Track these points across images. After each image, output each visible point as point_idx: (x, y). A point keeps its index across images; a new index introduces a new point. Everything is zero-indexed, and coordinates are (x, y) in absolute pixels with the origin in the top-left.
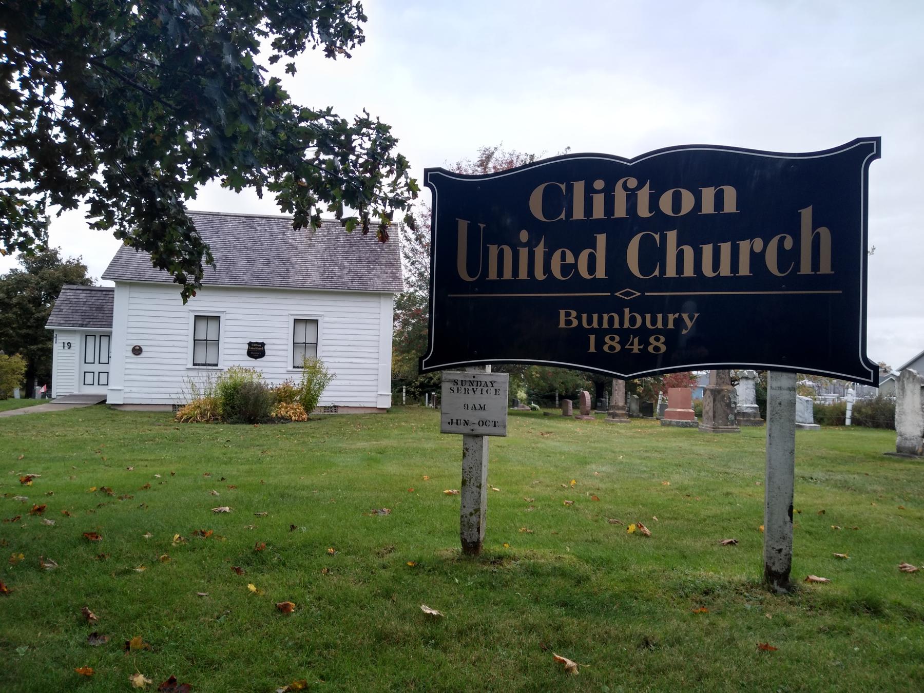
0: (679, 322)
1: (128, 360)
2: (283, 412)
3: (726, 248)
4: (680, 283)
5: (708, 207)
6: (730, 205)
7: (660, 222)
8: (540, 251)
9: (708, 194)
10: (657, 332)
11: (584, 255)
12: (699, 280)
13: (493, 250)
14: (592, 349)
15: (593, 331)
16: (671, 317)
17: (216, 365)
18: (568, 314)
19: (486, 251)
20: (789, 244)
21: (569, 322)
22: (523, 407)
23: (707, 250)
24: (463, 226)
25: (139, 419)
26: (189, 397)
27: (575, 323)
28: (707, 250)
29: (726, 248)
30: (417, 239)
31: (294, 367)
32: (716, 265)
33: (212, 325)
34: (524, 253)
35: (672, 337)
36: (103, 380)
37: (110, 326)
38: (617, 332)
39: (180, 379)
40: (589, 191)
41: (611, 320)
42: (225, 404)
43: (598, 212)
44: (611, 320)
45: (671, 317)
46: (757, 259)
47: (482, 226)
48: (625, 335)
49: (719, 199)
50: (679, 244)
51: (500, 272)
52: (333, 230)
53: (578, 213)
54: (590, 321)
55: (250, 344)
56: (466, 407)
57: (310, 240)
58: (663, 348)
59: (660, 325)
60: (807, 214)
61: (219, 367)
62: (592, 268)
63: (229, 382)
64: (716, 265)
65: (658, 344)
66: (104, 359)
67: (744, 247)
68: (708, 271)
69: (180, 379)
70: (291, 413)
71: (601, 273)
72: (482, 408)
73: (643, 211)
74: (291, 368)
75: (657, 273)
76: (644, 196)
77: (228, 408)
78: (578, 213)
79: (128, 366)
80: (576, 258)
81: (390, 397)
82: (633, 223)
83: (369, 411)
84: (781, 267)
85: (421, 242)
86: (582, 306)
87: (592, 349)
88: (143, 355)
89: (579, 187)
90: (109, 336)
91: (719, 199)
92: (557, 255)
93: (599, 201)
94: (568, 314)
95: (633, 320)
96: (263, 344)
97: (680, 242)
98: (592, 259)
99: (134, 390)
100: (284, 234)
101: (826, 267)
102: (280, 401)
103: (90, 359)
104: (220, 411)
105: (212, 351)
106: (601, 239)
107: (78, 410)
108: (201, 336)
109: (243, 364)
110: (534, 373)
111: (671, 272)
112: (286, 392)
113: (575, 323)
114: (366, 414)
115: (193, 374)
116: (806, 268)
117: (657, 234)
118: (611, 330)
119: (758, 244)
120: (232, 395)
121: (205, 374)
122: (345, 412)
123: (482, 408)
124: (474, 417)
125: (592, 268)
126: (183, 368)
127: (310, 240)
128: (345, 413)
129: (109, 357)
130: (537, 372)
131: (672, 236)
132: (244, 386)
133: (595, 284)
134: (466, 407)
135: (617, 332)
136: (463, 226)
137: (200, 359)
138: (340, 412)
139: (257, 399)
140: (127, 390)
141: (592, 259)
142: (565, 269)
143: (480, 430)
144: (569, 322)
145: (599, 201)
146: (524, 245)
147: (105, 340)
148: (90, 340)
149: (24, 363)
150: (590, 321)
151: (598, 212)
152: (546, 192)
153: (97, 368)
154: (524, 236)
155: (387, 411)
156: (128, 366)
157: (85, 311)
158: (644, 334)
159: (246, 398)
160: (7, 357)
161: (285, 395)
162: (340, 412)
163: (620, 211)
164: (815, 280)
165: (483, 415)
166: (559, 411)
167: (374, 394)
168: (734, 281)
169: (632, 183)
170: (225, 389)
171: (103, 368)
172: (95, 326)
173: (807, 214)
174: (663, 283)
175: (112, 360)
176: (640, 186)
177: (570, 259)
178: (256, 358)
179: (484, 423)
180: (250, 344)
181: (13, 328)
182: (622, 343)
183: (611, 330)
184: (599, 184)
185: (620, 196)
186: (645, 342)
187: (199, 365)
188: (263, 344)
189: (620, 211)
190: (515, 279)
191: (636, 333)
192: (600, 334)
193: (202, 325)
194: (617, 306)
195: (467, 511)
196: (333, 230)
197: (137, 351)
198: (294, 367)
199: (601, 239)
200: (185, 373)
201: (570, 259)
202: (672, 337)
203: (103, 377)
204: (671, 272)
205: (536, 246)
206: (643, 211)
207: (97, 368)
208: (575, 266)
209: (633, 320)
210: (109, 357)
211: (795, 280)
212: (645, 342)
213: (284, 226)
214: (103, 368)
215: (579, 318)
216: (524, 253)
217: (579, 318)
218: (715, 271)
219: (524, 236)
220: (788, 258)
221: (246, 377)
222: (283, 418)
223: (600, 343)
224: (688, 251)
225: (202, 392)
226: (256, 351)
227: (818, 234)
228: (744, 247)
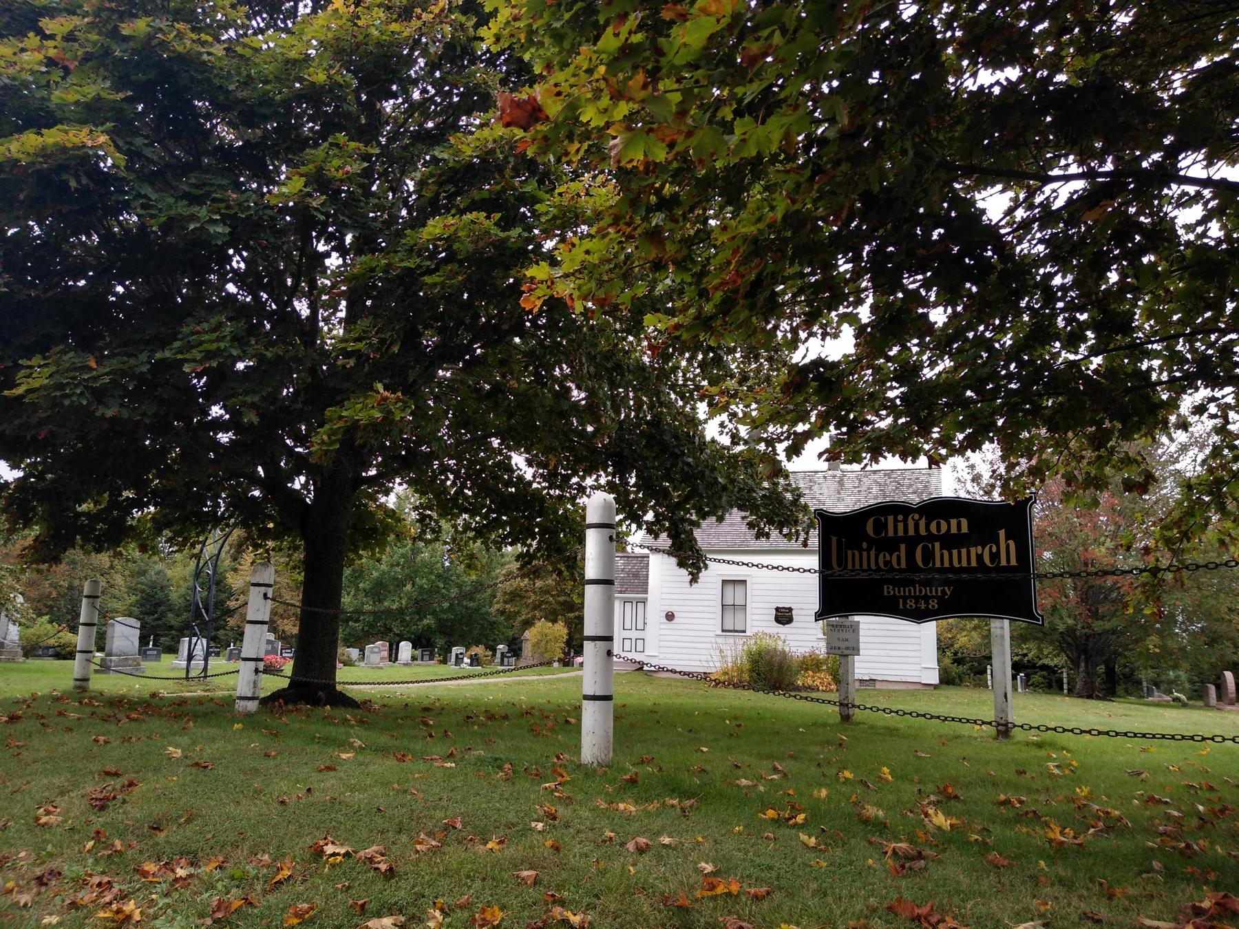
0: (944, 592)
1: (662, 626)
2: (809, 681)
3: (964, 551)
4: (942, 570)
5: (954, 530)
6: (965, 529)
7: (931, 538)
8: (873, 553)
9: (954, 522)
10: (933, 597)
11: (895, 555)
12: (952, 569)
13: (850, 553)
14: (901, 607)
15: (901, 597)
16: (939, 589)
17: (744, 632)
19: (846, 553)
20: (994, 549)
21: (889, 592)
22: (1160, 697)
23: (955, 552)
24: (834, 540)
25: (673, 683)
26: (718, 664)
27: (892, 593)
28: (955, 552)
29: (964, 551)
30: (973, 480)
31: (723, 631)
32: (960, 561)
33: (739, 589)
34: (865, 554)
35: (940, 599)
36: (640, 648)
37: (646, 592)
38: (913, 597)
39: (709, 646)
40: (896, 521)
41: (910, 590)
42: (752, 671)
43: (901, 533)
44: (910, 590)
45: (939, 589)
46: (980, 558)
48: (917, 599)
49: (959, 524)
50: (941, 549)
51: (1008, 560)
52: (865, 480)
53: (891, 533)
54: (899, 592)
55: (777, 609)
56: (839, 639)
57: (839, 493)
58: (936, 606)
59: (934, 594)
60: (1002, 533)
61: (748, 633)
62: (899, 563)
63: (754, 648)
64: (960, 561)
65: (934, 604)
66: (640, 626)
67: (973, 550)
68: (956, 564)
69: (709, 646)
70: (818, 682)
71: (903, 565)
72: (847, 640)
73: (923, 532)
74: (720, 633)
76: (922, 523)
77: (754, 674)
78: (891, 533)
79: (663, 632)
81: (937, 671)
82: (918, 538)
83: (911, 687)
84: (992, 561)
85: (978, 484)
86: (897, 583)
87: (901, 607)
88: (676, 620)
89: (891, 519)
90: (644, 602)
91: (959, 524)
92: (881, 555)
93: (901, 526)
95: (920, 591)
96: (790, 609)
97: (941, 549)
98: (899, 558)
99: (668, 656)
100: (810, 489)
101: (1013, 562)
102: (807, 670)
103: (628, 626)
104: (746, 676)
105: (739, 616)
106: (903, 547)
107: (619, 674)
108: (729, 601)
109: (767, 631)
110: (1151, 647)
111: (938, 565)
112: (812, 660)
113: (892, 593)
114: (907, 691)
115: (720, 640)
116: (1004, 563)
118: (910, 597)
119: (980, 548)
120: (757, 662)
121: (731, 641)
122: (884, 686)
123: (847, 640)
124: (843, 645)
125: (899, 563)
126: (712, 634)
127: (839, 493)
128: (884, 688)
129: (645, 623)
130: (1155, 646)
131: (937, 545)
132: (768, 652)
133: (901, 571)
134: (839, 639)
135: (913, 597)
136: (834, 540)
137: (729, 626)
138: (878, 686)
139: (781, 666)
140: (662, 656)
141: (899, 558)
142: (886, 563)
143: (846, 652)
144: (889, 592)
145: (901, 526)
146: (864, 550)
147: (640, 606)
148: (628, 606)
149: (566, 631)
150: (899, 592)
151: (901, 533)
152: (875, 521)
153: (634, 634)
154: (865, 545)
155: (935, 687)
156: (663, 632)
157: (623, 578)
158: (927, 598)
159: (770, 664)
160: (550, 624)
161: (811, 664)
162: (878, 686)
163: (911, 532)
164: (1009, 568)
165: (847, 644)
166: (1201, 703)
167: (918, 667)
168: (969, 570)
169: (917, 516)
170: (750, 653)
171: (639, 634)
172: (632, 592)
173: (1002, 533)
174: (934, 569)
175: (648, 627)
176: (920, 519)
177: (888, 558)
178: (784, 624)
179: (847, 648)
180: (777, 609)
181: (552, 596)
182: (916, 603)
183: (910, 597)
184: (900, 517)
185: (911, 523)
186: (927, 603)
187: (729, 631)
188: (790, 609)
189: (911, 532)
191: (923, 598)
192: (905, 598)
193: (729, 589)
194: (912, 583)
195: (842, 698)
196: (865, 480)
197: (670, 617)
198: (723, 631)
199: (903, 547)
200: (713, 640)
201: (888, 558)
202: (940, 599)
203: (640, 643)
204: (938, 565)
206: (923, 532)
207: (634, 634)
208: (890, 561)
209: (920, 591)
210: (645, 623)
211: (999, 569)
212: (927, 603)
213: (811, 481)
214: (639, 634)
215: (894, 590)
216: (865, 554)
217: (894, 590)
219: (865, 545)
221: (771, 643)
222: (810, 687)
223: (905, 603)
224: (946, 553)
225: (730, 659)
226: (784, 616)
228: (973, 550)
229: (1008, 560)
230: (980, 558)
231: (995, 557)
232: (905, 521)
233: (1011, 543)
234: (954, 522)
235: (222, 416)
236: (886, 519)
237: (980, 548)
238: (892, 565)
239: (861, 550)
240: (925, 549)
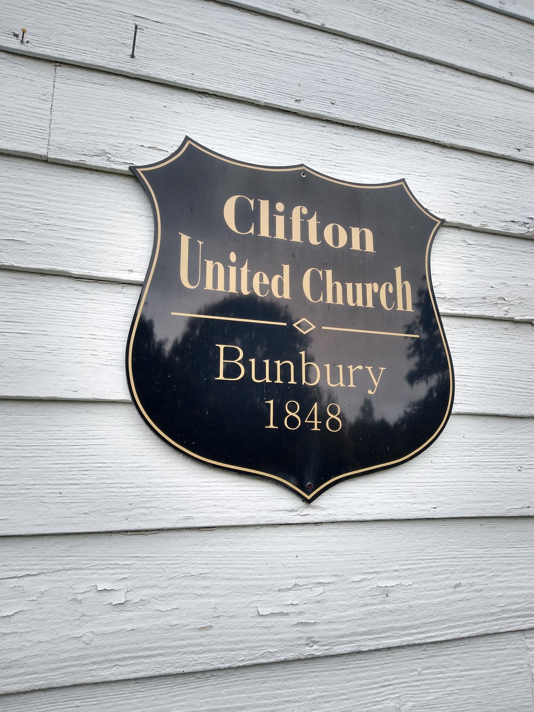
8: (245, 270)
9: (356, 232)
11: (276, 278)
13: (210, 264)
18: (231, 354)
20: (391, 290)
21: (232, 370)
34: (233, 270)
40: (273, 211)
46: (376, 297)
47: (201, 243)
49: (362, 237)
51: (405, 306)
60: (398, 271)
67: (369, 286)
75: (321, 299)
80: (270, 280)
84: (389, 305)
91: (362, 237)
92: (257, 276)
94: (231, 354)
98: (281, 283)
116: (400, 308)
117: (252, 200)
141: (281, 283)
142: (263, 288)
144: (232, 370)
145: (280, 221)
146: (233, 265)
173: (398, 271)
184: (280, 207)
190: (227, 291)
201: (266, 281)
205: (242, 266)
208: (269, 286)
218: (216, 265)
220: (392, 298)
224: (339, 285)
227: (404, 284)
228: (369, 286)
229: (405, 306)
230: (376, 297)
231: (392, 298)
232: (288, 214)
233: (407, 283)
234: (356, 232)
235: (439, 378)
236: (257, 205)
237: (376, 285)
238: (271, 293)
239: (227, 263)
240: (314, 277)
